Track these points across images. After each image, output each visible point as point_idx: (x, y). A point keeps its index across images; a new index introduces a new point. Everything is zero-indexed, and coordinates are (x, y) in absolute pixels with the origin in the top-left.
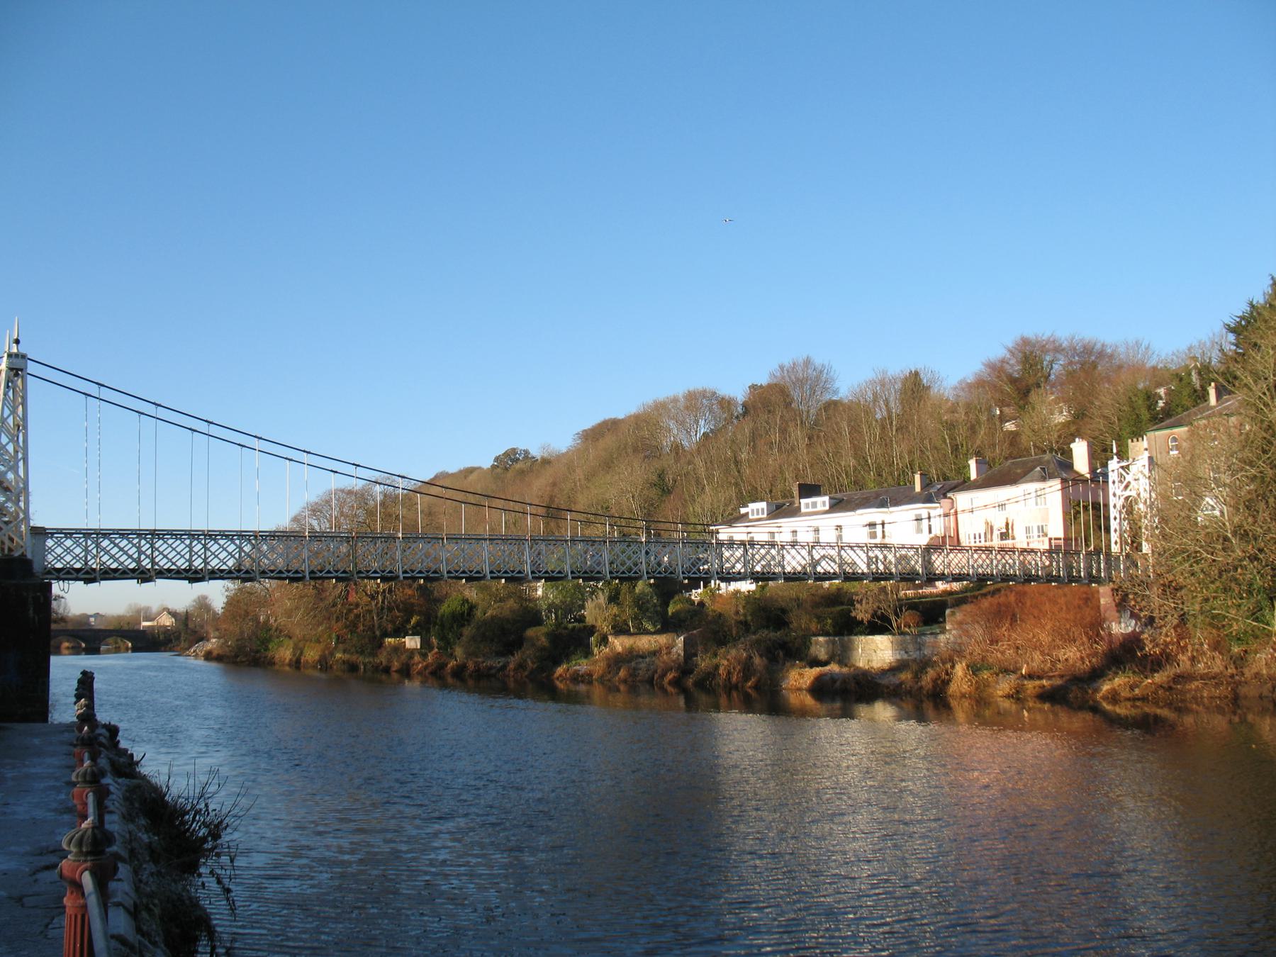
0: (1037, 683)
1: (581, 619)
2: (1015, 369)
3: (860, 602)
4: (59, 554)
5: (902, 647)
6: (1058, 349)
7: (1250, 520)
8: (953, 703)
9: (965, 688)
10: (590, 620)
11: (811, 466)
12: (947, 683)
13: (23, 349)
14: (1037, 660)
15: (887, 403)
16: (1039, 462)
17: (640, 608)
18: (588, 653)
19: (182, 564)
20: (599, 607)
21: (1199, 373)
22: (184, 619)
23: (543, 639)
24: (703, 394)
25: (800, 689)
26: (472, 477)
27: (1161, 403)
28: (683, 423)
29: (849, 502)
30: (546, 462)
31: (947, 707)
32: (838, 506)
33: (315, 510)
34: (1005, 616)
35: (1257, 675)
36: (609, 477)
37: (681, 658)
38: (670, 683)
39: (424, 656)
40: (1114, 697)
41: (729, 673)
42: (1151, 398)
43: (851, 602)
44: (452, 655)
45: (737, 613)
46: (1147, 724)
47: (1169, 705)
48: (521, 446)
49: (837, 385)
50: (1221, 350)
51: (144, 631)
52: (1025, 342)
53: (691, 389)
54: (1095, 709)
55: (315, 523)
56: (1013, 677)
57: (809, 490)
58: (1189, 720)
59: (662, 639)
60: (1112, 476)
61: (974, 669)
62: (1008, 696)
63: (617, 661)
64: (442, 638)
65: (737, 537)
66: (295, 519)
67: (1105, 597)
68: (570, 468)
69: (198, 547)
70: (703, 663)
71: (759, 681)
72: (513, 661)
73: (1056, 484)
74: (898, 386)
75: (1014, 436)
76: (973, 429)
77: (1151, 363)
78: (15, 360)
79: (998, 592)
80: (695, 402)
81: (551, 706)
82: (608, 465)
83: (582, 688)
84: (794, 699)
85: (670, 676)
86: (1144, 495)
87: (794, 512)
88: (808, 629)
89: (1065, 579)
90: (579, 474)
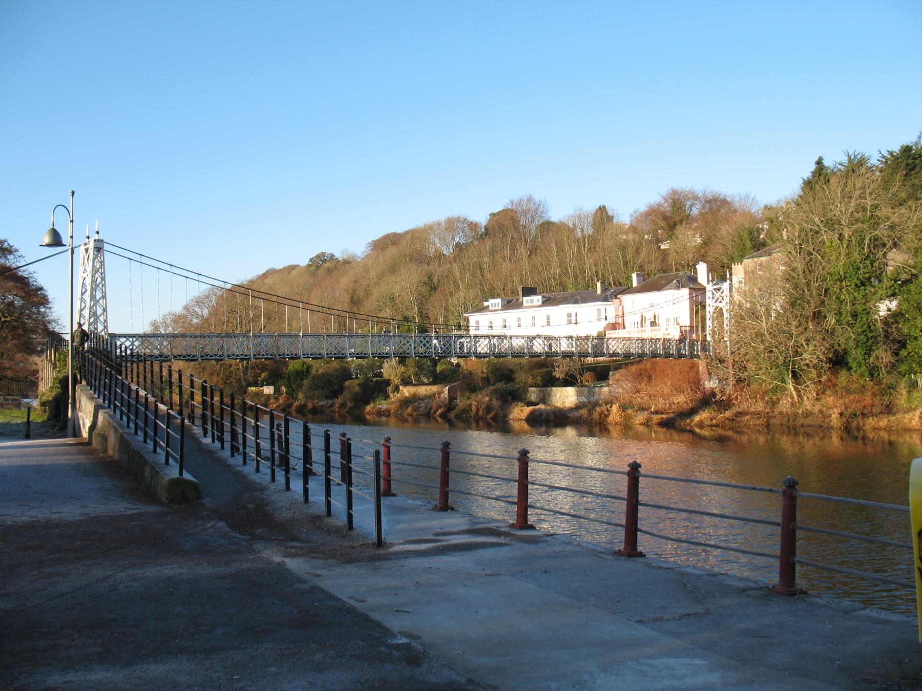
0: (660, 416)
1: (380, 375)
3: (558, 367)
5: (579, 394)
6: (696, 198)
8: (611, 428)
9: (618, 419)
10: (386, 376)
11: (531, 273)
12: (607, 416)
13: (101, 237)
14: (661, 403)
16: (676, 277)
17: (419, 368)
18: (387, 397)
20: (392, 367)
23: (358, 388)
24: (458, 220)
25: (521, 420)
26: (294, 273)
28: (444, 239)
29: (555, 299)
30: (346, 262)
31: (607, 430)
32: (547, 302)
33: (199, 302)
34: (645, 376)
35: (781, 413)
36: (394, 278)
37: (447, 401)
38: (440, 416)
39: (277, 399)
40: (701, 425)
41: (478, 409)
43: (553, 367)
44: (296, 399)
45: (482, 372)
46: (722, 440)
47: (732, 429)
48: (328, 250)
52: (675, 192)
53: (450, 216)
54: (691, 432)
56: (646, 413)
57: (529, 291)
58: (745, 438)
59: (434, 388)
61: (623, 408)
62: (642, 424)
63: (406, 402)
64: (289, 387)
66: (186, 308)
67: (702, 366)
68: (366, 270)
70: (461, 402)
71: (496, 414)
72: (338, 401)
73: (685, 292)
74: (590, 220)
75: (665, 253)
76: (637, 251)
79: (642, 362)
80: (452, 224)
81: (364, 427)
82: (393, 269)
83: (384, 419)
84: (516, 426)
85: (439, 411)
87: (519, 305)
88: (526, 383)
89: (681, 355)
90: (373, 274)
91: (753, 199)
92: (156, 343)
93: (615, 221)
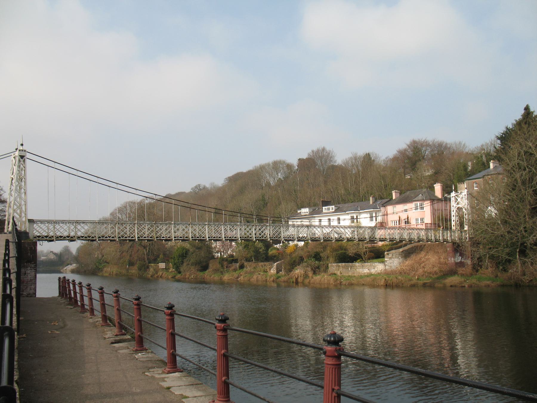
2: (410, 153)
4: (38, 230)
7: (508, 217)
13: (24, 148)
15: (357, 166)
19: (66, 234)
21: (486, 156)
22: (60, 256)
27: (470, 168)
42: (465, 167)
49: (336, 158)
50: (495, 147)
51: (42, 261)
52: (414, 142)
53: (275, 160)
55: (120, 216)
57: (326, 203)
60: (453, 199)
65: (305, 223)
66: (112, 214)
69: (72, 227)
77: (467, 150)
78: (21, 152)
80: (276, 165)
86: (466, 207)
87: (320, 212)
91: (464, 145)
92: (65, 227)
93: (375, 162)
